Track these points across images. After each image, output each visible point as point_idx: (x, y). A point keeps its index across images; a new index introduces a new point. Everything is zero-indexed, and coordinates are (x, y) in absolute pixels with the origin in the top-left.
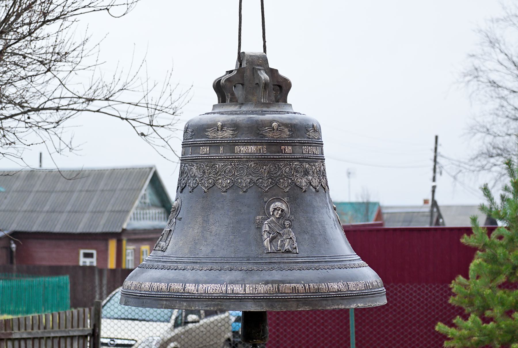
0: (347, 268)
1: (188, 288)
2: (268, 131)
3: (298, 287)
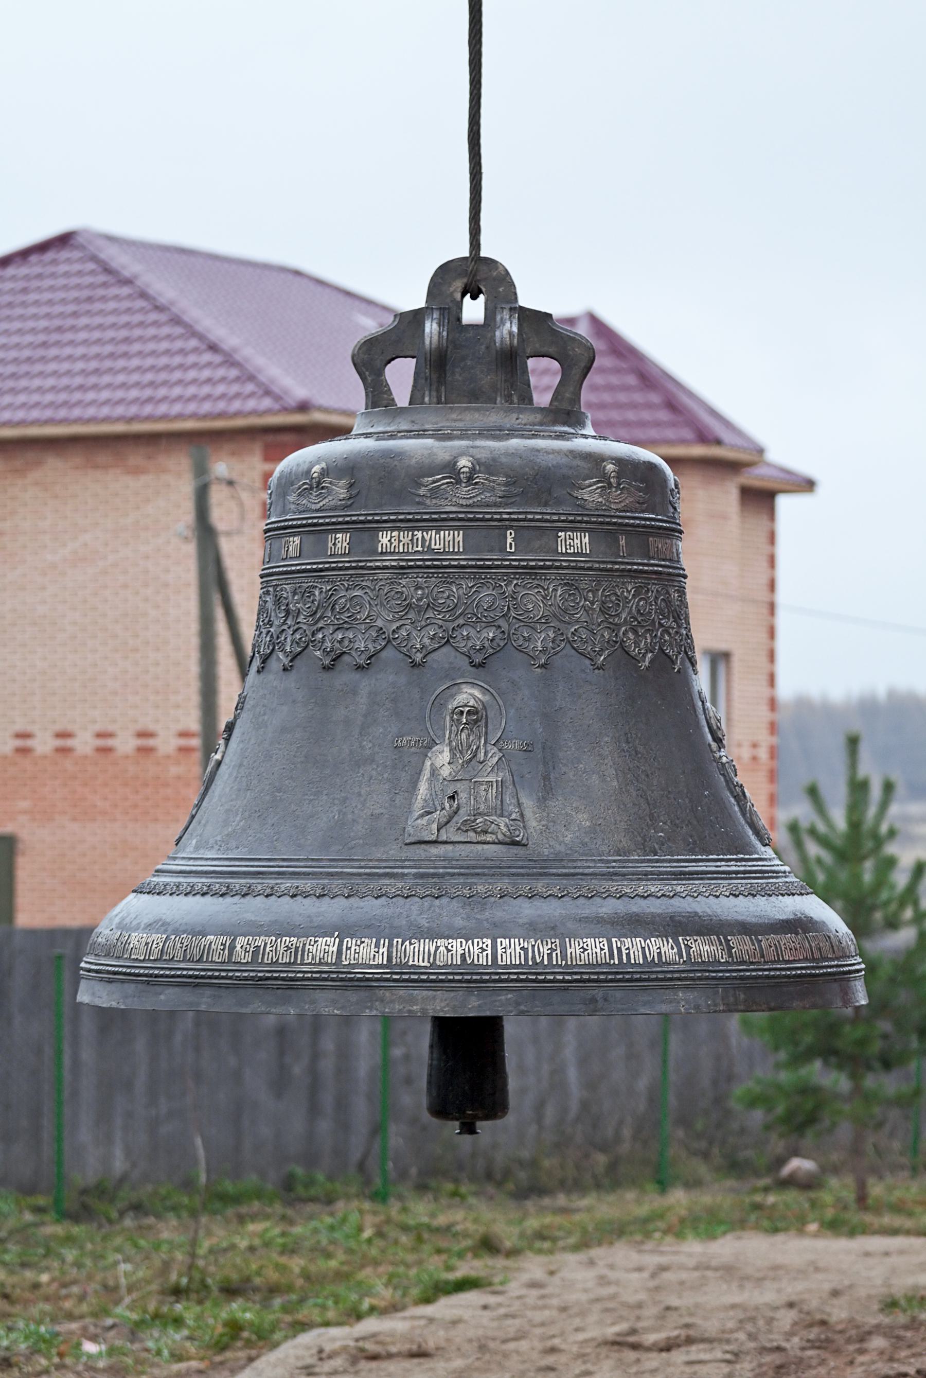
0: (755, 896)
1: (594, 950)
2: (443, 484)
3: (659, 948)
